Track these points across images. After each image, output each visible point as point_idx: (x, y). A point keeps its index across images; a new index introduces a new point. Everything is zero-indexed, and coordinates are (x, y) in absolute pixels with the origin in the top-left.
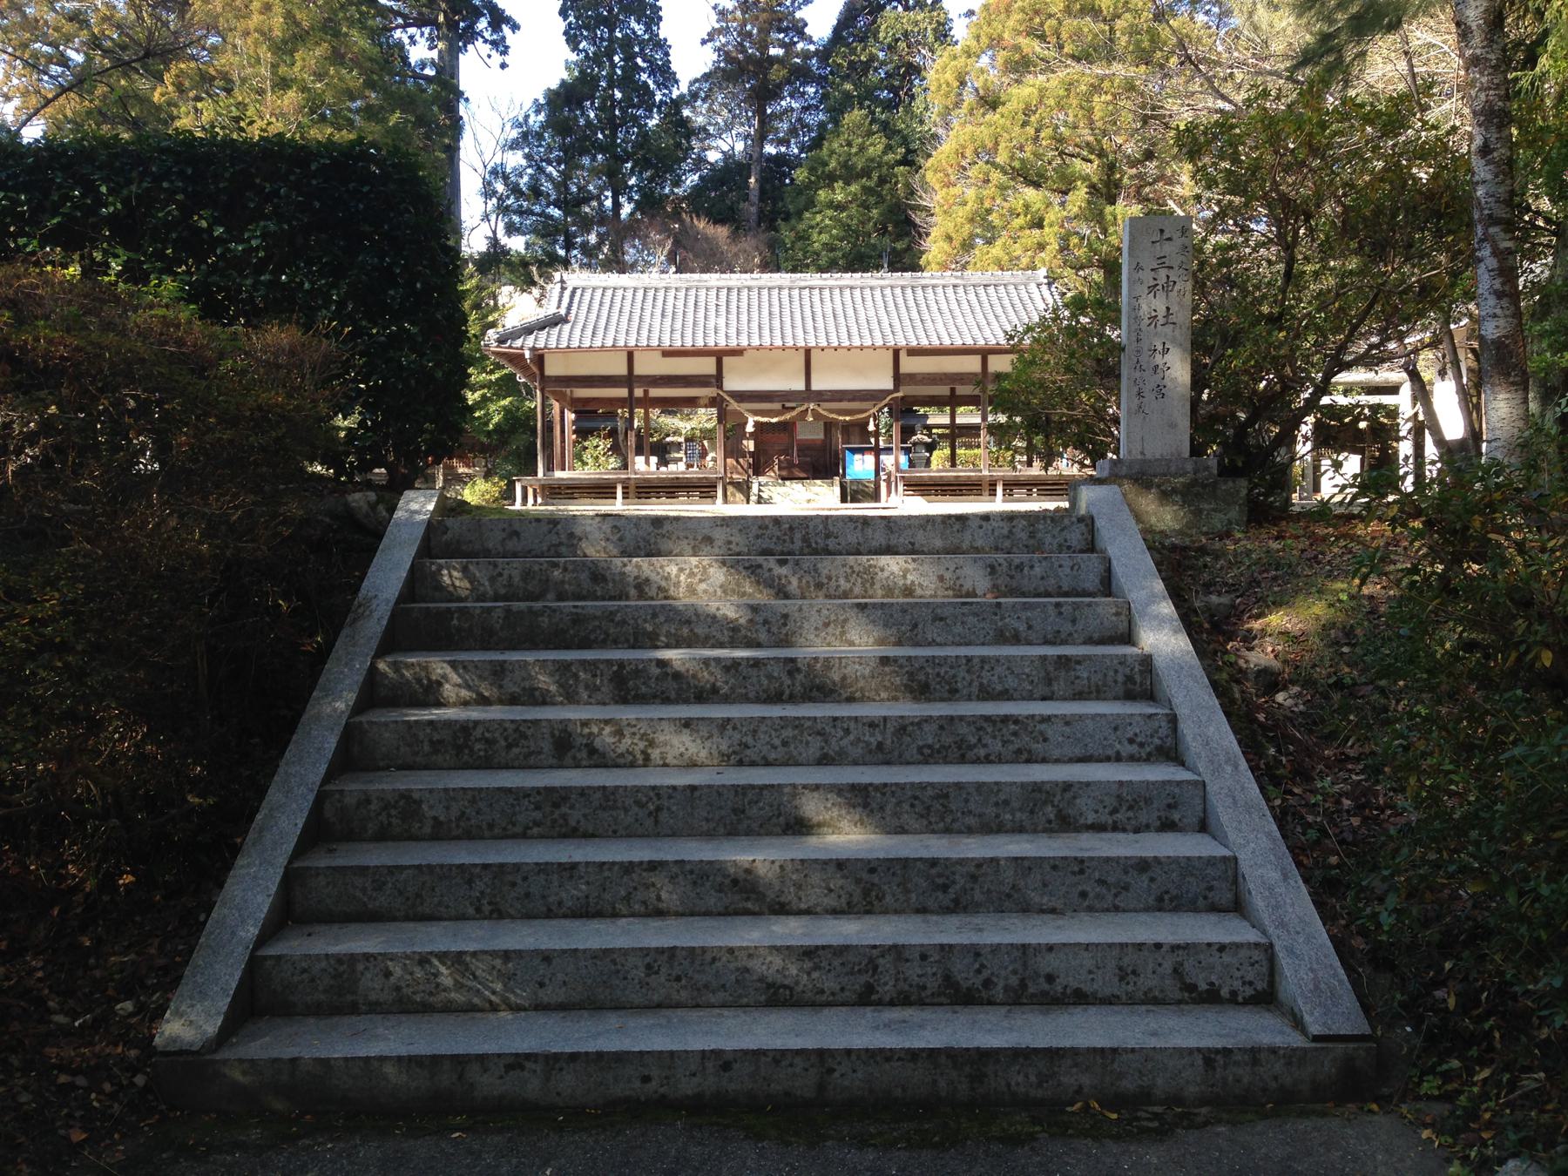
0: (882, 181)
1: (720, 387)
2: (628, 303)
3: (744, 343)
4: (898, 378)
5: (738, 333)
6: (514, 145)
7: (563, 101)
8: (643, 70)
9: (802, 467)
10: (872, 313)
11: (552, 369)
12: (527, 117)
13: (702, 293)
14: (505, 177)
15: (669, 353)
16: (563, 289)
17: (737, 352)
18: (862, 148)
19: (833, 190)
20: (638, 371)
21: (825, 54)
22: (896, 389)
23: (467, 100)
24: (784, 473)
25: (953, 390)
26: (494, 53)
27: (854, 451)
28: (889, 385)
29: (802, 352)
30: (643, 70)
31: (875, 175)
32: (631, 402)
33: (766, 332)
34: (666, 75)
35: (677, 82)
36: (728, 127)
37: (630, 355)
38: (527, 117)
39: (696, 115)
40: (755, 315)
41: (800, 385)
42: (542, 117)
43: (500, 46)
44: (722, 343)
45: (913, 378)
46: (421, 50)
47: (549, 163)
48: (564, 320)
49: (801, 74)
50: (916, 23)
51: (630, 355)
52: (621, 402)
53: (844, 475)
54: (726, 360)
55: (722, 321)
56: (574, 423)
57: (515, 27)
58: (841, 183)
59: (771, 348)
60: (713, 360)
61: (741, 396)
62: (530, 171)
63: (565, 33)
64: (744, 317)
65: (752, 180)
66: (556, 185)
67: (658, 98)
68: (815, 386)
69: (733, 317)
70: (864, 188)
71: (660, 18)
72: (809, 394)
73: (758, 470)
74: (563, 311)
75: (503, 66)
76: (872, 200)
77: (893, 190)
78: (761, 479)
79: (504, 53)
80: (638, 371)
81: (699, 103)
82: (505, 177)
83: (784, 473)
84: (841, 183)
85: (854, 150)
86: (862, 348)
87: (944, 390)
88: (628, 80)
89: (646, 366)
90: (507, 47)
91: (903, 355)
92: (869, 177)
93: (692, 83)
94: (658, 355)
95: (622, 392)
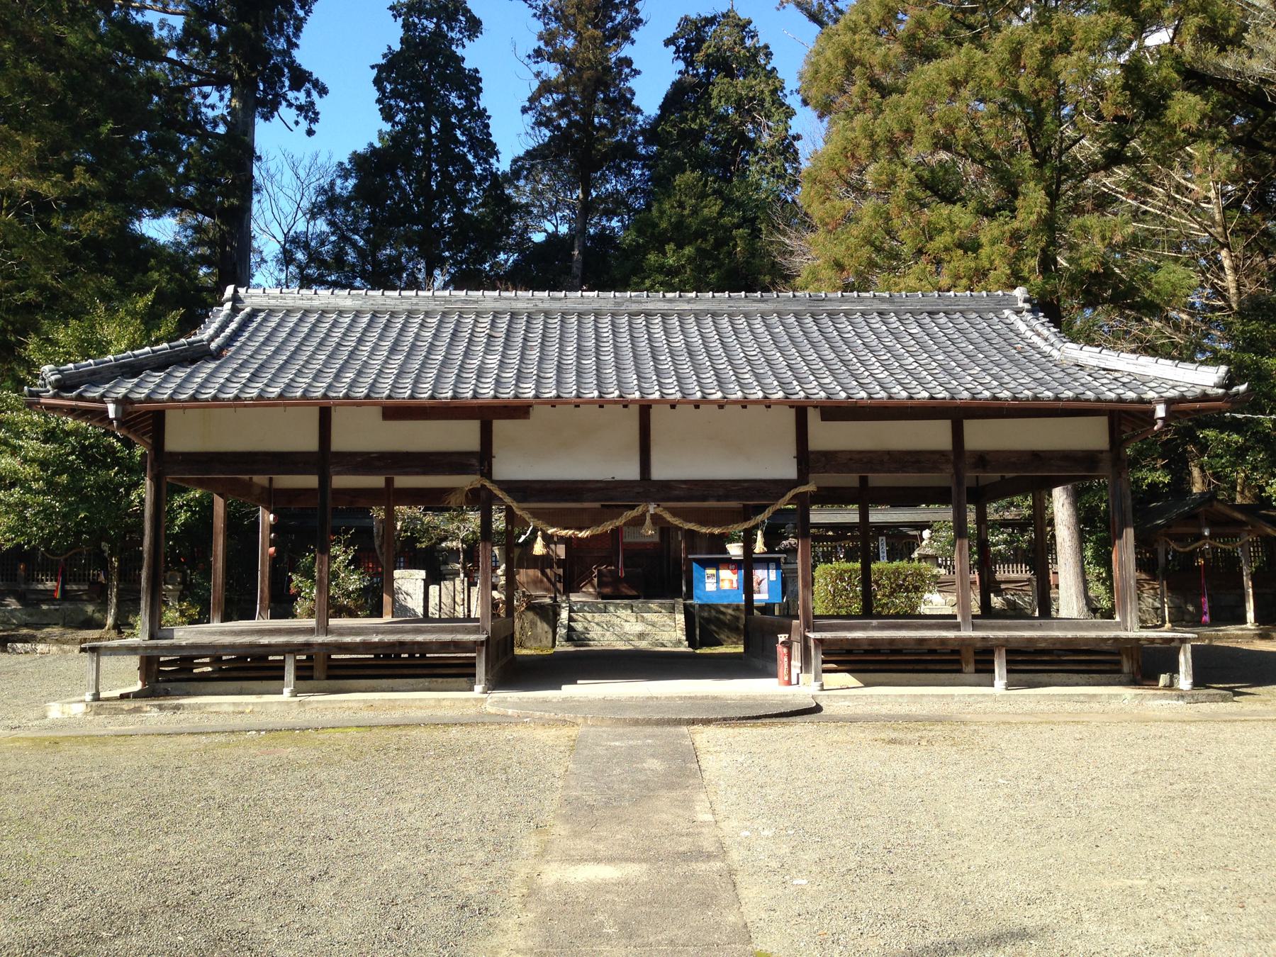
0: (719, 244)
1: (487, 474)
2: (338, 333)
3: (529, 391)
4: (806, 459)
5: (520, 377)
6: (314, 212)
7: (368, 166)
8: (463, 144)
9: (629, 580)
10: (753, 351)
11: (180, 438)
12: (332, 184)
13: (469, 320)
14: (306, 246)
15: (395, 412)
16: (235, 310)
17: (518, 410)
18: (695, 212)
19: (665, 254)
20: (339, 443)
21: (652, 133)
22: (802, 478)
23: (259, 158)
24: (607, 590)
25: (864, 480)
26: (301, 119)
27: (706, 564)
28: (791, 472)
29: (635, 409)
30: (463, 144)
31: (711, 239)
32: (391, 496)
33: (571, 378)
34: (487, 148)
35: (497, 153)
36: (554, 209)
37: (325, 415)
38: (332, 184)
39: (521, 193)
40: (554, 350)
41: (629, 471)
42: (351, 182)
43: (309, 112)
44: (487, 391)
45: (831, 460)
46: (216, 104)
47: (356, 231)
48: (217, 355)
49: (627, 152)
50: (751, 88)
51: (325, 415)
52: (373, 495)
53: (690, 595)
54: (499, 426)
55: (493, 361)
56: (273, 528)
57: (323, 91)
58: (672, 246)
59: (579, 402)
60: (474, 426)
61: (523, 490)
62: (333, 238)
63: (379, 101)
64: (534, 354)
65: (576, 253)
66: (360, 252)
67: (478, 170)
68: (658, 473)
69: (515, 353)
70: (698, 250)
71: (480, 90)
72: (647, 488)
73: (571, 586)
74: (213, 346)
75: (310, 132)
76: (708, 263)
77: (730, 254)
78: (574, 597)
79: (315, 120)
80: (339, 443)
81: (522, 183)
82: (306, 246)
83: (607, 590)
84: (672, 246)
85: (686, 212)
86: (745, 403)
87: (850, 480)
88: (449, 157)
89: (355, 434)
90: (317, 114)
91: (813, 416)
92: (705, 240)
93: (515, 161)
94: (377, 411)
95: (377, 481)
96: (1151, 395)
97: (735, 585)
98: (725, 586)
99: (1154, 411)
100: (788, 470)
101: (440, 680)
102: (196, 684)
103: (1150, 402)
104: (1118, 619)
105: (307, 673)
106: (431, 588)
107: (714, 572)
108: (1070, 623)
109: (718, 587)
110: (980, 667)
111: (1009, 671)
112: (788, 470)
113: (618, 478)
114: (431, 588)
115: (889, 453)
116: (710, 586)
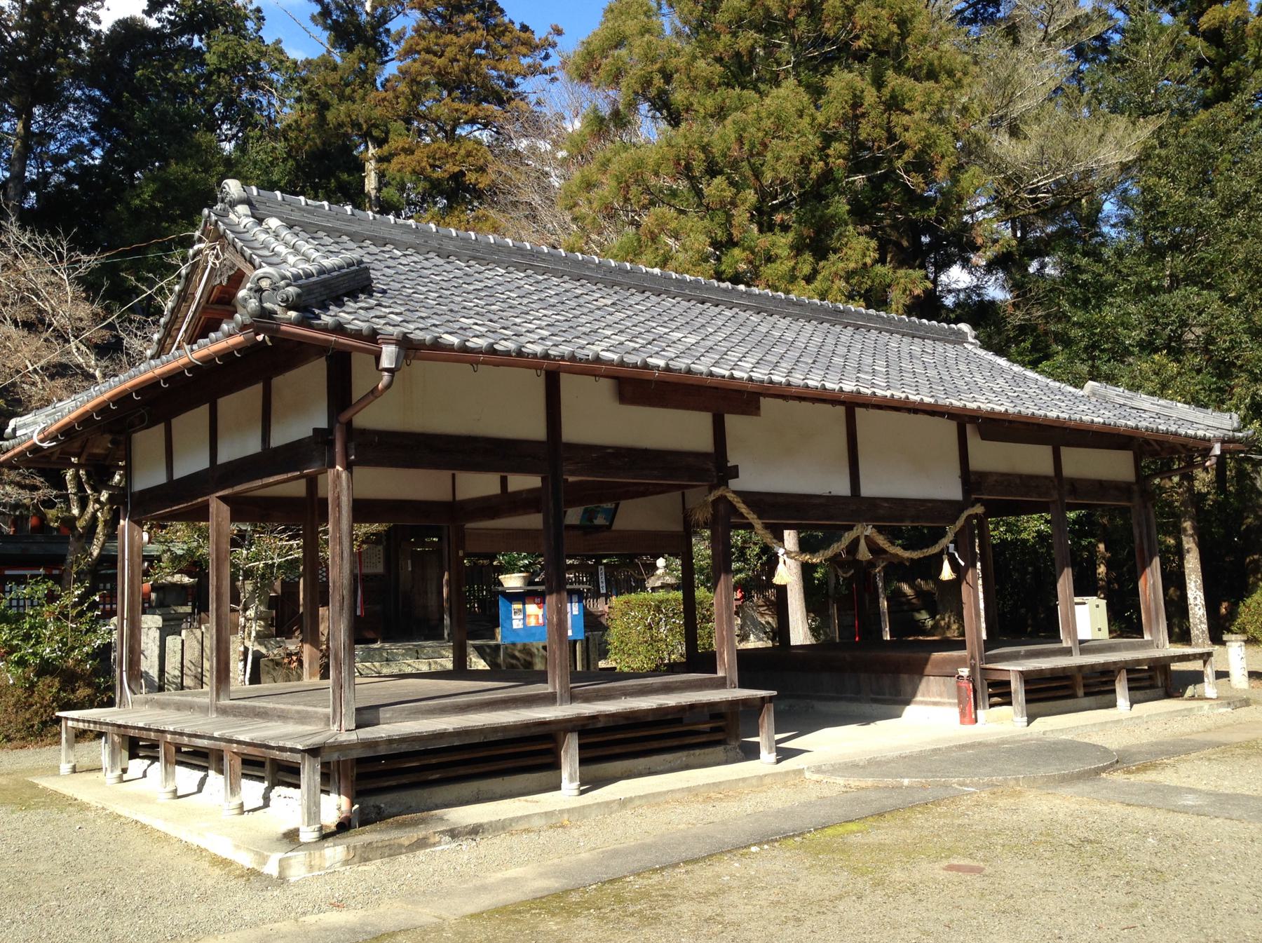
4: (971, 480)
20: (573, 432)
41: (841, 487)
68: (867, 490)
89: (595, 420)
96: (1209, 434)
97: (541, 621)
98: (532, 622)
99: (1211, 449)
100: (952, 490)
101: (697, 752)
102: (419, 792)
103: (1209, 440)
104: (1147, 637)
105: (369, 768)
106: (169, 639)
107: (520, 606)
108: (1086, 647)
109: (524, 624)
110: (1133, 685)
111: (1130, 689)
112: (952, 490)
113: (834, 493)
114: (169, 639)
115: (1020, 476)
116: (517, 624)
